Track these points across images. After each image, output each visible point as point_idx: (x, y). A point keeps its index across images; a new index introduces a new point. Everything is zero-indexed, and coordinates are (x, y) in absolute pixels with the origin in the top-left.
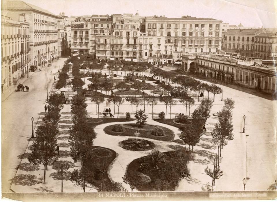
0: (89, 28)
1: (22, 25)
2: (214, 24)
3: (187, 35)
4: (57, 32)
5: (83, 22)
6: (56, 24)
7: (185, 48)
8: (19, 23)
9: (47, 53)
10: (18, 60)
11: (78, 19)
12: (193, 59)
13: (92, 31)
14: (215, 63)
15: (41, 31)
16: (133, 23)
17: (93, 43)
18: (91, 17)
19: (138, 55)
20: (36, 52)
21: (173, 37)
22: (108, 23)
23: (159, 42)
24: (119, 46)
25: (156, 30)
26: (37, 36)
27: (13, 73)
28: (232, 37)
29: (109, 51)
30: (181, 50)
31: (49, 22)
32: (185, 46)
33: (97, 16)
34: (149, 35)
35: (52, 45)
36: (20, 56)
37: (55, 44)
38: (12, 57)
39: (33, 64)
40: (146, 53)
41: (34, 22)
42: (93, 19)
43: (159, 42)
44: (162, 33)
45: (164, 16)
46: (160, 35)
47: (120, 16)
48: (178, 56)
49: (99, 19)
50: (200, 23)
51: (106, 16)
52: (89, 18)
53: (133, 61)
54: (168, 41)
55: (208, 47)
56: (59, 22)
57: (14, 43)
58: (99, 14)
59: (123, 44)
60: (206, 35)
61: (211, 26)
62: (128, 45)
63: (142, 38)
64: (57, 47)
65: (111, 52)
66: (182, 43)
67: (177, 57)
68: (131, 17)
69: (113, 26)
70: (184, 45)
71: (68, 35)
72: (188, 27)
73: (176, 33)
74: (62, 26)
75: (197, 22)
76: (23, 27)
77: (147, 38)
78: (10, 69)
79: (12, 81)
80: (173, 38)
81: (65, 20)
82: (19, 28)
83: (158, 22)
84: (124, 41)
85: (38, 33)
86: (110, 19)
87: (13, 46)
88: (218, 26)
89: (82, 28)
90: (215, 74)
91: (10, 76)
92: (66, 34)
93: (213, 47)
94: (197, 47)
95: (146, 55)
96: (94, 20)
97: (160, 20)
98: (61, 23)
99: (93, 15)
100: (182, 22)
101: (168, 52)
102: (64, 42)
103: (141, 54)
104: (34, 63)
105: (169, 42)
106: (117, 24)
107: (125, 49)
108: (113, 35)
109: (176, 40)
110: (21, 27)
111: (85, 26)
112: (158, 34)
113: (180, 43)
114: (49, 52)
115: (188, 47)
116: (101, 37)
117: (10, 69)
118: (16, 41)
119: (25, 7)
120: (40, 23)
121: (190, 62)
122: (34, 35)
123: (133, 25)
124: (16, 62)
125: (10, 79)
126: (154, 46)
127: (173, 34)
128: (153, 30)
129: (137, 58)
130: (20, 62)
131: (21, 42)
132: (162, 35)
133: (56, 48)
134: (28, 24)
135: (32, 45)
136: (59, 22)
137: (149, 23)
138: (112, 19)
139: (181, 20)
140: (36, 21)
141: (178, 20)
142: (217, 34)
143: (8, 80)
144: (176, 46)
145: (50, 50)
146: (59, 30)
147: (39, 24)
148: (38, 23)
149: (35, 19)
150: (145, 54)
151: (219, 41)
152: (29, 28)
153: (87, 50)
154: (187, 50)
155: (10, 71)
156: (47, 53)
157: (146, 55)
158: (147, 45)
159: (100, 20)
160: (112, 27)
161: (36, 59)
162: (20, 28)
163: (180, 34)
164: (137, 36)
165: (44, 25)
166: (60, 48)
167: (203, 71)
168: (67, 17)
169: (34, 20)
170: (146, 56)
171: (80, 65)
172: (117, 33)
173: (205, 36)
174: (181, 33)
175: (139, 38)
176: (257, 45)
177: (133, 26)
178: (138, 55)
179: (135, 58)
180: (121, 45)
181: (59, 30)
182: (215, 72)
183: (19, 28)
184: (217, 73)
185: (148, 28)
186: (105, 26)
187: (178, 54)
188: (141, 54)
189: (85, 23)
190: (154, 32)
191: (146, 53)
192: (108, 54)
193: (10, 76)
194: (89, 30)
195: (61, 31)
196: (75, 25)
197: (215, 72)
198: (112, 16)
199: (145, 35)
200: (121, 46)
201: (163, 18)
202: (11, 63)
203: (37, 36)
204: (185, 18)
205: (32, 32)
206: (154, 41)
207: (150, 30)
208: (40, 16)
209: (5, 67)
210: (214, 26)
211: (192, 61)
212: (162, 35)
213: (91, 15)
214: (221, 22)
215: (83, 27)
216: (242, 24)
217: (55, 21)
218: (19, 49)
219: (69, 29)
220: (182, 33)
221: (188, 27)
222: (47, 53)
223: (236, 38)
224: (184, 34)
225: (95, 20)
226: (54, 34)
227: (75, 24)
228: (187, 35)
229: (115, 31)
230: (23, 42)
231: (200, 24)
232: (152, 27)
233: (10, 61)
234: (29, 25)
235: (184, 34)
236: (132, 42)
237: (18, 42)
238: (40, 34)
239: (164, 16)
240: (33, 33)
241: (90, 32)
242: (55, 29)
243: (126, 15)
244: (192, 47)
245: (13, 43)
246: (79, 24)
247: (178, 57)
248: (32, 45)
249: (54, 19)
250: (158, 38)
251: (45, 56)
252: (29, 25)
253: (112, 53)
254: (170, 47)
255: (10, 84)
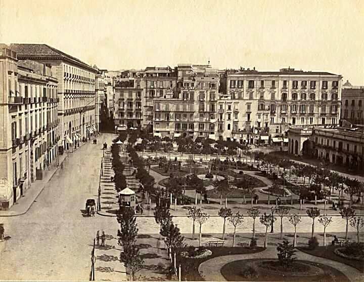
0: (142, 88)
1: (50, 82)
2: (330, 81)
3: (290, 97)
4: (94, 94)
5: (133, 79)
6: (94, 81)
7: (286, 118)
8: (44, 78)
9: (82, 126)
10: (43, 139)
11: (125, 74)
12: (308, 135)
13: (146, 92)
14: (348, 143)
15: (73, 92)
16: (209, 80)
17: (148, 110)
18: (144, 71)
19: (216, 128)
20: (66, 124)
21: (268, 101)
22: (171, 80)
23: (249, 107)
24: (188, 115)
25: (242, 90)
26: (69, 99)
27: (36, 160)
28: (349, 100)
29: (173, 123)
30: (280, 121)
31: (85, 79)
32: (287, 114)
33: (154, 68)
34: (233, 98)
35: (88, 113)
36: (46, 132)
37: (92, 112)
38: (36, 135)
39: (62, 143)
40: (229, 125)
41: (64, 78)
42: (147, 74)
43: (249, 107)
44: (252, 95)
45: (254, 68)
46: (248, 98)
47: (189, 69)
48: (277, 130)
49: (156, 73)
50: (309, 79)
51: (167, 69)
52: (141, 73)
53: (210, 138)
54: (261, 107)
55: (321, 116)
56: (96, 78)
57: (38, 111)
58: (157, 66)
59: (194, 112)
60: (318, 97)
61: (325, 84)
62: (202, 113)
63: (20, 85)
64: (93, 116)
65: (176, 124)
66: (281, 110)
67: (275, 131)
68: (204, 71)
69: (180, 84)
70: (285, 114)
71: (110, 97)
72: (290, 85)
73: (273, 95)
74: (101, 85)
75: (300, 79)
76: (50, 86)
77: (231, 103)
78: (32, 154)
79: (35, 174)
80: (267, 102)
81: (103, 75)
82: (45, 87)
83: (245, 78)
84: (196, 107)
85: (69, 95)
86: (172, 74)
87: (36, 115)
88: (335, 85)
89: (132, 88)
90: (348, 159)
91: (32, 166)
92: (106, 95)
93: (316, 116)
94: (325, 116)
95: (229, 128)
96: (149, 76)
97: (248, 75)
98: (99, 79)
99: (147, 68)
100: (282, 77)
101: (261, 124)
102: (104, 106)
103: (221, 127)
104: (63, 142)
105: (263, 109)
106: (186, 80)
107: (196, 119)
108: (180, 97)
109: (272, 105)
110: (48, 85)
111: (135, 85)
112: (246, 96)
113: (278, 111)
114: (84, 124)
115: (291, 116)
116: (160, 100)
117: (32, 154)
118: (40, 108)
119: (49, 53)
120: (72, 79)
121: (303, 140)
122: (64, 99)
123: (209, 82)
124: (40, 142)
125: (32, 170)
126: (240, 115)
127: (267, 96)
128: (239, 90)
129: (215, 133)
130: (45, 142)
131: (47, 109)
132: (251, 98)
133: (93, 118)
134: (55, 80)
135: (61, 114)
136: (96, 78)
137: (232, 79)
138: (177, 74)
139: (281, 74)
140: (67, 76)
141: (276, 75)
142: (335, 96)
143: (30, 172)
144: (273, 114)
145: (85, 122)
146: (97, 90)
147: (70, 81)
148: (70, 79)
149: (65, 73)
150: (227, 127)
151: (337, 107)
152: (57, 86)
153: (139, 122)
154: (298, 122)
155: (32, 158)
156: (81, 125)
157: (229, 128)
158: (231, 113)
159: (158, 74)
160: (177, 84)
161: (66, 135)
162: (46, 87)
163: (278, 97)
164: (216, 99)
165: (77, 82)
166: (98, 118)
167: (324, 154)
168: (106, 70)
169: (63, 75)
170: (229, 130)
171: (128, 141)
172: (185, 95)
173: (317, 99)
174: (280, 94)
175: (218, 102)
176: (363, 108)
177: (210, 84)
178: (216, 128)
179: (212, 133)
180: (192, 113)
181: (97, 90)
182: (348, 156)
183: (45, 87)
184: (350, 157)
185: (231, 88)
186: (167, 83)
187: (278, 127)
188: (221, 127)
189: (136, 79)
190: (240, 94)
191: (229, 125)
192: (171, 127)
193: (32, 166)
194: (143, 89)
195: (99, 92)
196: (121, 83)
197: (348, 156)
198: (176, 68)
199: (227, 97)
200: (192, 115)
201: (253, 72)
202: (34, 144)
203: (69, 99)
204: (285, 72)
205: (62, 93)
206: (241, 106)
207: (234, 90)
208: (67, 66)
209: (26, 151)
210: (330, 84)
211: (306, 139)
212: (251, 98)
213: (144, 68)
214: (340, 77)
215: (133, 86)
216: (349, 82)
217: (92, 76)
218: (44, 123)
219: (110, 89)
220: (281, 94)
221: (290, 85)
222: (81, 125)
223: (357, 102)
224: (284, 96)
225: (149, 74)
226: (90, 96)
227: (120, 81)
228: (290, 97)
229: (182, 91)
230: (50, 108)
231: (309, 80)
232: (236, 86)
233: (32, 142)
234: (57, 82)
235: (284, 96)
236: (207, 108)
237: (44, 109)
238: (73, 97)
239: (254, 68)
240: (63, 94)
241: (143, 94)
242: (92, 89)
243: (196, 68)
244: (287, 116)
245: (26, 113)
246: (127, 81)
247: (277, 132)
248: (61, 114)
249: (91, 73)
250: (247, 103)
251: (78, 130)
252: (57, 82)
253: (178, 125)
254: (265, 116)
255: (32, 178)
